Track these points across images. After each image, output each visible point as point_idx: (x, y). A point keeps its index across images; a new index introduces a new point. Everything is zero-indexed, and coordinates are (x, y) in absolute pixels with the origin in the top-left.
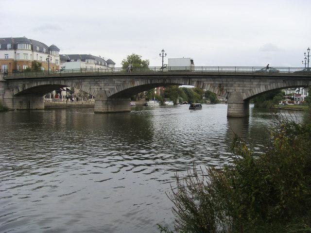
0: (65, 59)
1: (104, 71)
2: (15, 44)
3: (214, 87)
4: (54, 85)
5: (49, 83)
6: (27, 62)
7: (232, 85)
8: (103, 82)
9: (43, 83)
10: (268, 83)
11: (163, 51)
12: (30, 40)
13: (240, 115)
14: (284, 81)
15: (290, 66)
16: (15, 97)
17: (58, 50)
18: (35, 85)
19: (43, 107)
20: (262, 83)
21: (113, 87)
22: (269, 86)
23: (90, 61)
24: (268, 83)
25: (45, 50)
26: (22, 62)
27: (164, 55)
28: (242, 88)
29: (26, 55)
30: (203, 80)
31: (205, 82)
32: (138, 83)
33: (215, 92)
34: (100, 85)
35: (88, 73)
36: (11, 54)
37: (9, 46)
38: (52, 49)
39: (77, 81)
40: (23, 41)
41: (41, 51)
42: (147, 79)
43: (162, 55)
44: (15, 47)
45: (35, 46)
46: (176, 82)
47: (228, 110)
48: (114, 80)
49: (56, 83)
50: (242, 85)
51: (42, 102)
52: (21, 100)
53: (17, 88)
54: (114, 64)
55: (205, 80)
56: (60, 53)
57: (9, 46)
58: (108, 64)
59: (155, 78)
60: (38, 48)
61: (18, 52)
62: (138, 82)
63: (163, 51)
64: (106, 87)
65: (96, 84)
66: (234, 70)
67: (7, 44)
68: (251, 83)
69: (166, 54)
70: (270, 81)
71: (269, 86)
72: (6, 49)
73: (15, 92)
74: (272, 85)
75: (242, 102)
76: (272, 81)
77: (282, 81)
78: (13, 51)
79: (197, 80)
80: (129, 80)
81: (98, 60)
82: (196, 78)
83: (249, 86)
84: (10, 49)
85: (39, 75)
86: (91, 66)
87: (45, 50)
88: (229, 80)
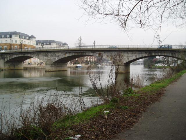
0: (38, 42)
2: (10, 35)
4: (25, 56)
5: (22, 55)
6: (17, 44)
8: (50, 55)
9: (20, 56)
11: (95, 41)
12: (19, 33)
13: (123, 72)
15: (168, 44)
17: (35, 38)
19: (23, 68)
20: (133, 54)
21: (55, 57)
23: (55, 44)
25: (27, 38)
26: (14, 44)
27: (81, 39)
29: (16, 41)
30: (102, 53)
31: (103, 54)
34: (49, 56)
35: (37, 50)
36: (8, 41)
37: (8, 36)
38: (31, 38)
39: (37, 54)
40: (15, 33)
41: (5, 37)
43: (157, 38)
44: (11, 37)
45: (21, 36)
48: (55, 53)
49: (26, 55)
53: (7, 58)
54: (68, 45)
55: (103, 53)
56: (37, 39)
57: (8, 36)
58: (64, 45)
60: (23, 37)
61: (12, 39)
62: (68, 54)
63: (95, 41)
64: (51, 57)
65: (46, 56)
67: (2, 35)
70: (138, 53)
72: (6, 37)
73: (6, 60)
74: (139, 55)
75: (123, 65)
76: (139, 53)
77: (145, 53)
78: (9, 39)
79: (99, 53)
81: (59, 43)
82: (98, 52)
83: (126, 56)
84: (9, 38)
85: (12, 51)
86: (55, 46)
87: (27, 38)
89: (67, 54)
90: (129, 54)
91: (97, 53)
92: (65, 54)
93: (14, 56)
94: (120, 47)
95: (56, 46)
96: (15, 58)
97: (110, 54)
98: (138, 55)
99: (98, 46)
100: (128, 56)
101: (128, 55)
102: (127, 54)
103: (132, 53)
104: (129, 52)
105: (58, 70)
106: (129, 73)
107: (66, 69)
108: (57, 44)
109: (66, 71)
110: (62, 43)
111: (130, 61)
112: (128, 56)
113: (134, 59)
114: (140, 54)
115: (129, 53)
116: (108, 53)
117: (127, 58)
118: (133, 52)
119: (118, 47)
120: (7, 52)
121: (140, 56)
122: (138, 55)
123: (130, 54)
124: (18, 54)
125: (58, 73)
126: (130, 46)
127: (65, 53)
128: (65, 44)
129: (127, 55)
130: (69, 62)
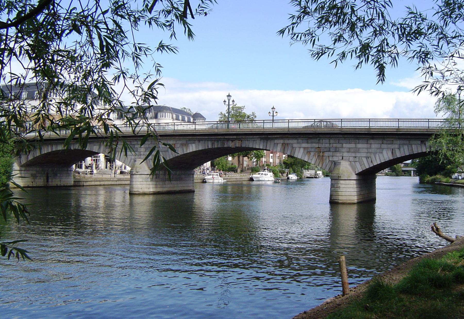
1: (171, 128)
3: (309, 152)
7: (336, 150)
10: (397, 146)
14: (421, 141)
16: (23, 169)
18: (38, 154)
20: (384, 146)
22: (397, 151)
24: (397, 146)
27: (275, 114)
28: (354, 155)
30: (291, 141)
32: (192, 148)
33: (309, 161)
42: (208, 140)
43: (227, 103)
46: (257, 147)
47: (331, 191)
50: (352, 150)
51: (68, 175)
52: (34, 172)
55: (295, 141)
59: (228, 140)
62: (194, 145)
63: (273, 108)
66: (425, 125)
68: (369, 146)
69: (233, 101)
70: (398, 142)
71: (397, 151)
74: (402, 149)
76: (402, 142)
77: (419, 142)
79: (281, 141)
80: (180, 142)
82: (281, 138)
88: (332, 141)
89: (190, 145)
90: (373, 146)
91: (276, 141)
92: (186, 145)
93: (46, 150)
94: (346, 125)
95: (171, 121)
96: (48, 154)
97: (317, 145)
98: (399, 148)
99: (283, 121)
100: (370, 151)
101: (370, 148)
102: (365, 146)
103: (381, 142)
104: (373, 138)
105: (165, 190)
106: (374, 200)
107: (191, 188)
108: (174, 116)
109: (190, 195)
110: (188, 114)
111: (374, 167)
112: (370, 151)
113: (387, 160)
114: (406, 147)
115: (371, 141)
116: (310, 141)
117: (367, 158)
118: (384, 138)
119: (339, 124)
120: (202, 130)
121: (405, 151)
122: (399, 148)
123: (375, 145)
124: (57, 144)
125: (171, 197)
126: (376, 120)
127: (184, 142)
128: (197, 116)
129: (367, 148)
130: (208, 164)
